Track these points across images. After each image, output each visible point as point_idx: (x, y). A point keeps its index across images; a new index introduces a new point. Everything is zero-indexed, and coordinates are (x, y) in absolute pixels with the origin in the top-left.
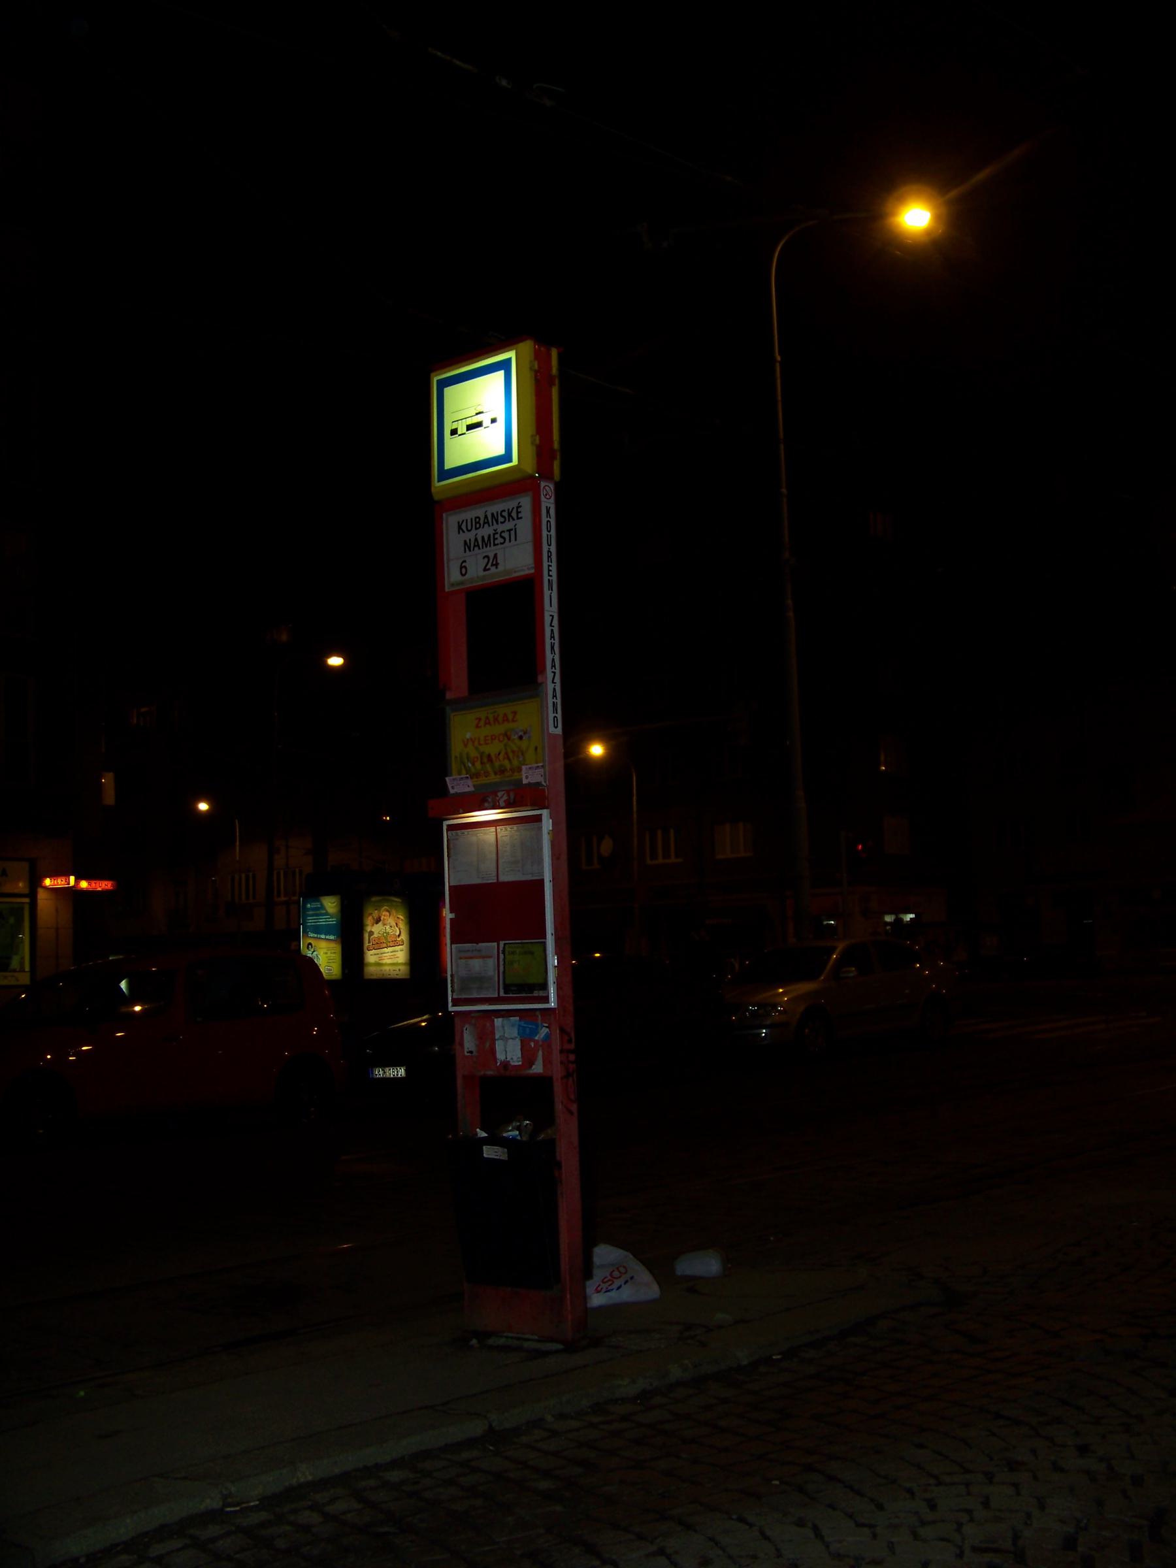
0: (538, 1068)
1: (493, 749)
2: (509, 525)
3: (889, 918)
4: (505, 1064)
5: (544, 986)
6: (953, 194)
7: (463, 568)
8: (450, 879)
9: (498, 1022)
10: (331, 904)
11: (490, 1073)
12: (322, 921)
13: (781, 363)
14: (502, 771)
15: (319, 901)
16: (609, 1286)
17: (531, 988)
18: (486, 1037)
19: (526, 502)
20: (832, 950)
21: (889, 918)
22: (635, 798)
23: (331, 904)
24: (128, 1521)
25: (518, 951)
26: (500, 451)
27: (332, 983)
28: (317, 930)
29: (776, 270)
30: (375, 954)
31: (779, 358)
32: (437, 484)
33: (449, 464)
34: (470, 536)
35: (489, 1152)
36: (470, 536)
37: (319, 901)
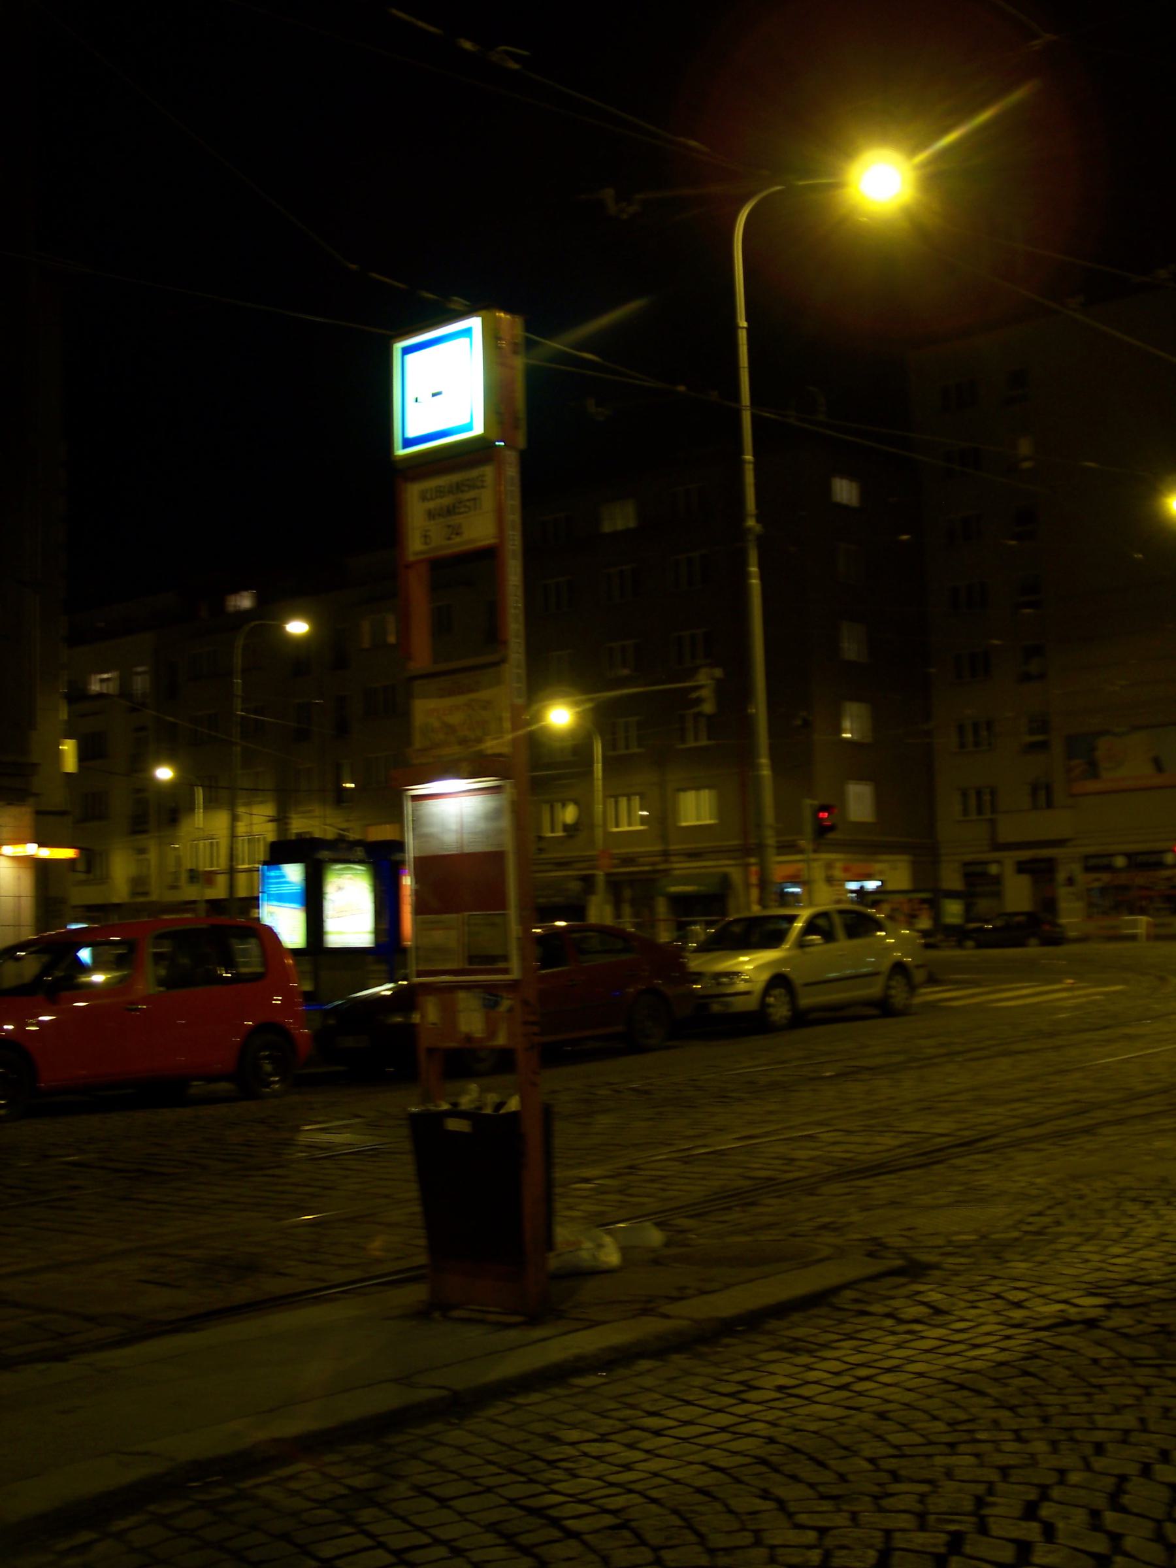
0: (501, 1040)
1: (455, 719)
2: (472, 494)
3: (853, 886)
4: (469, 1038)
5: (505, 958)
6: (922, 157)
7: (426, 537)
8: (411, 851)
9: (461, 995)
10: (293, 873)
11: (453, 1045)
12: (285, 890)
13: (749, 330)
14: (463, 742)
15: (279, 869)
16: (665, 1515)
17: (493, 959)
18: (449, 1013)
19: (488, 471)
20: (792, 919)
21: (853, 886)
22: (420, 24)
23: (293, 873)
24: (601, 806)
25: (402, 1489)
26: (409, 357)
27: (296, 952)
28: (281, 898)
29: (496, 911)
30: (342, 911)
31: (745, 324)
32: (400, 452)
33: (411, 433)
34: (431, 505)
35: (453, 1125)
36: (431, 505)
37: (279, 869)
